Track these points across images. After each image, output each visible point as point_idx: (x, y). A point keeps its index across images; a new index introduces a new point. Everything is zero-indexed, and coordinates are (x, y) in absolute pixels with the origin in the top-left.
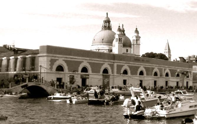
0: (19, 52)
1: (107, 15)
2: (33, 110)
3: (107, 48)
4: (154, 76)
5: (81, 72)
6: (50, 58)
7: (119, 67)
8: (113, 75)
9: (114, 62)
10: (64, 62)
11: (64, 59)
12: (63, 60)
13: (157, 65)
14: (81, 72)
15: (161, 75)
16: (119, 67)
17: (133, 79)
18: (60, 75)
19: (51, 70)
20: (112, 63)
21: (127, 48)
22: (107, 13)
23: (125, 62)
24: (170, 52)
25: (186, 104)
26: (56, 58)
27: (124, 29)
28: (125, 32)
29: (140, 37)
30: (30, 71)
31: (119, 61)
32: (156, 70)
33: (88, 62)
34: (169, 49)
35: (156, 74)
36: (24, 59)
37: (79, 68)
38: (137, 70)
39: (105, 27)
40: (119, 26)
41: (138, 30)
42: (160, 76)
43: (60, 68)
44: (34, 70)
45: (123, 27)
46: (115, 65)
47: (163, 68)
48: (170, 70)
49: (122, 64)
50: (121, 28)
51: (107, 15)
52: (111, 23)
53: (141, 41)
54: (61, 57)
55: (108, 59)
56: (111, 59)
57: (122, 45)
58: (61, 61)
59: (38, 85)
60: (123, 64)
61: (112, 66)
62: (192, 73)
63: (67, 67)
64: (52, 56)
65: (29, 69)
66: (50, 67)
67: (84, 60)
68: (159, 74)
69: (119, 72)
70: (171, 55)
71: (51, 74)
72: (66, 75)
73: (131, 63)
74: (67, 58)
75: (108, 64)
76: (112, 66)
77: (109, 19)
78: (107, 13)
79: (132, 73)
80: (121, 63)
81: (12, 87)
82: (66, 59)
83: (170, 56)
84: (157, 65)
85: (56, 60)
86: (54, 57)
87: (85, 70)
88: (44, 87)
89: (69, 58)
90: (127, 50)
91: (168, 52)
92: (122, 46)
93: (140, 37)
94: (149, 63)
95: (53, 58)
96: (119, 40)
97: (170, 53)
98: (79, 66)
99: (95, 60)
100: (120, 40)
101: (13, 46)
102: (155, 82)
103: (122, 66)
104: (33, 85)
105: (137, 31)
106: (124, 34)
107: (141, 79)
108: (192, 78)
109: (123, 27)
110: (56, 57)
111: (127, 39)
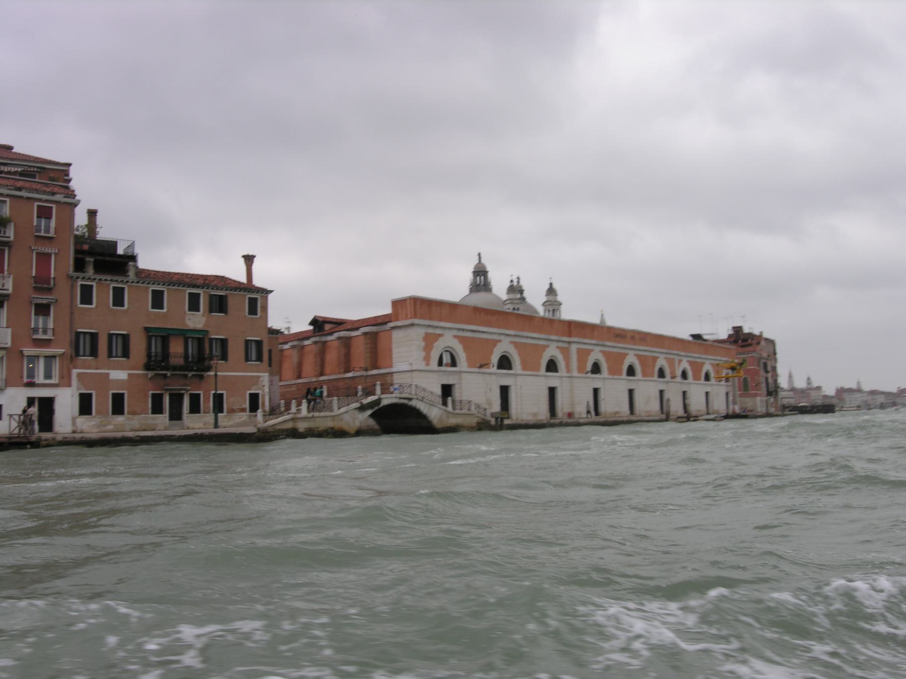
0: (327, 327)
7: (583, 355)
8: (568, 375)
9: (570, 342)
11: (455, 333)
12: (455, 337)
13: (664, 351)
16: (583, 355)
17: (473, 421)
19: (428, 364)
20: (566, 345)
22: (479, 254)
26: (438, 331)
28: (525, 294)
30: (366, 370)
31: (581, 340)
32: (661, 362)
35: (661, 374)
36: (347, 343)
37: (492, 358)
40: (512, 281)
41: (555, 286)
44: (378, 368)
45: (518, 282)
46: (574, 348)
48: (690, 363)
50: (515, 284)
52: (490, 275)
54: (450, 328)
55: (557, 335)
56: (564, 335)
59: (406, 401)
64: (429, 326)
65: (363, 365)
66: (423, 354)
67: (502, 338)
69: (581, 369)
73: (608, 343)
74: (463, 330)
75: (558, 347)
76: (565, 352)
77: (484, 267)
78: (479, 254)
80: (588, 343)
81: (339, 408)
82: (461, 334)
84: (664, 351)
86: (432, 326)
87: (505, 363)
88: (423, 407)
89: (468, 330)
94: (647, 346)
95: (430, 331)
99: (527, 337)
101: (288, 328)
103: (589, 352)
104: (394, 401)
109: (518, 282)
110: (437, 327)
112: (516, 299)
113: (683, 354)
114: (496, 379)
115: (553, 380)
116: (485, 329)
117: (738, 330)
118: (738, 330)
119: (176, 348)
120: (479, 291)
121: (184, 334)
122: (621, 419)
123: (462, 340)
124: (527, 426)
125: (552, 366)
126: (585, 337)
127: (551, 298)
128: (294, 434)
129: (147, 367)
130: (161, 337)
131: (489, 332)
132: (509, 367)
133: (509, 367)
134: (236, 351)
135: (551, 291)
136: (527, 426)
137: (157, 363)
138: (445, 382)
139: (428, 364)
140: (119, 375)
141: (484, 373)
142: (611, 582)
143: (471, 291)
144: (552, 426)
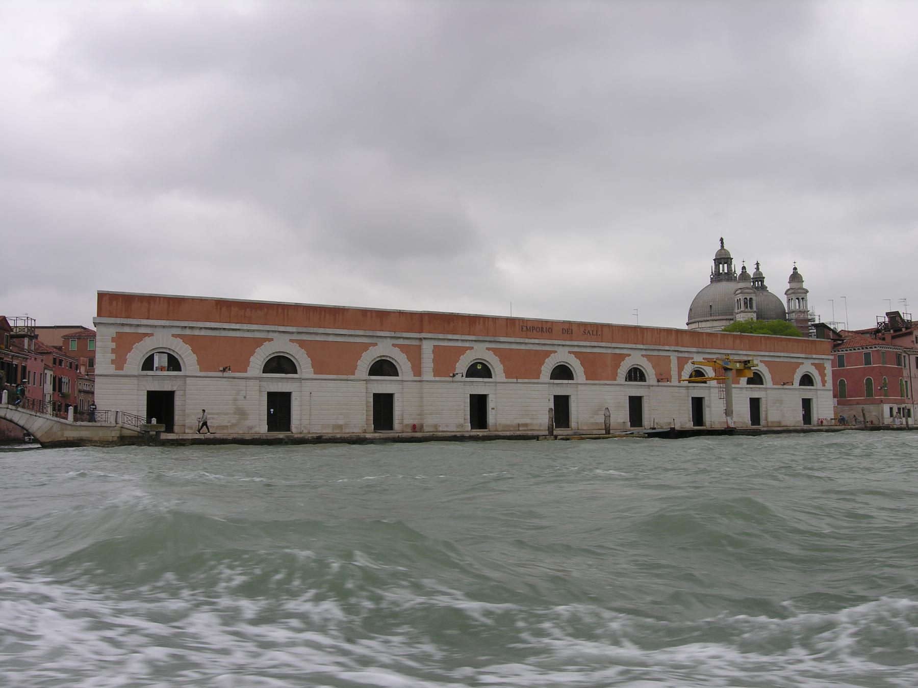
2: (514, 465)
4: (552, 381)
5: (143, 370)
10: (573, 356)
14: (143, 370)
17: (114, 434)
19: (120, 367)
20: (416, 343)
22: (722, 240)
23: (473, 338)
25: (481, 494)
29: (807, 292)
31: (441, 336)
33: (812, 364)
42: (658, 381)
46: (427, 348)
49: (459, 344)
60: (800, 361)
61: (414, 355)
63: (432, 365)
71: (116, 380)
72: (712, 390)
76: (414, 355)
77: (727, 253)
78: (722, 240)
79: (509, 373)
93: (807, 292)
96: (745, 303)
98: (542, 363)
102: (807, 404)
106: (764, 288)
108: (829, 384)
110: (138, 326)
112: (747, 288)
113: (694, 350)
114: (742, 395)
116: (226, 326)
117: (894, 316)
118: (894, 316)
120: (720, 281)
122: (530, 433)
124: (319, 440)
125: (383, 368)
126: (454, 332)
127: (795, 285)
135: (795, 277)
136: (319, 440)
138: (156, 387)
139: (120, 367)
141: (234, 378)
143: (712, 281)
144: (804, 431)
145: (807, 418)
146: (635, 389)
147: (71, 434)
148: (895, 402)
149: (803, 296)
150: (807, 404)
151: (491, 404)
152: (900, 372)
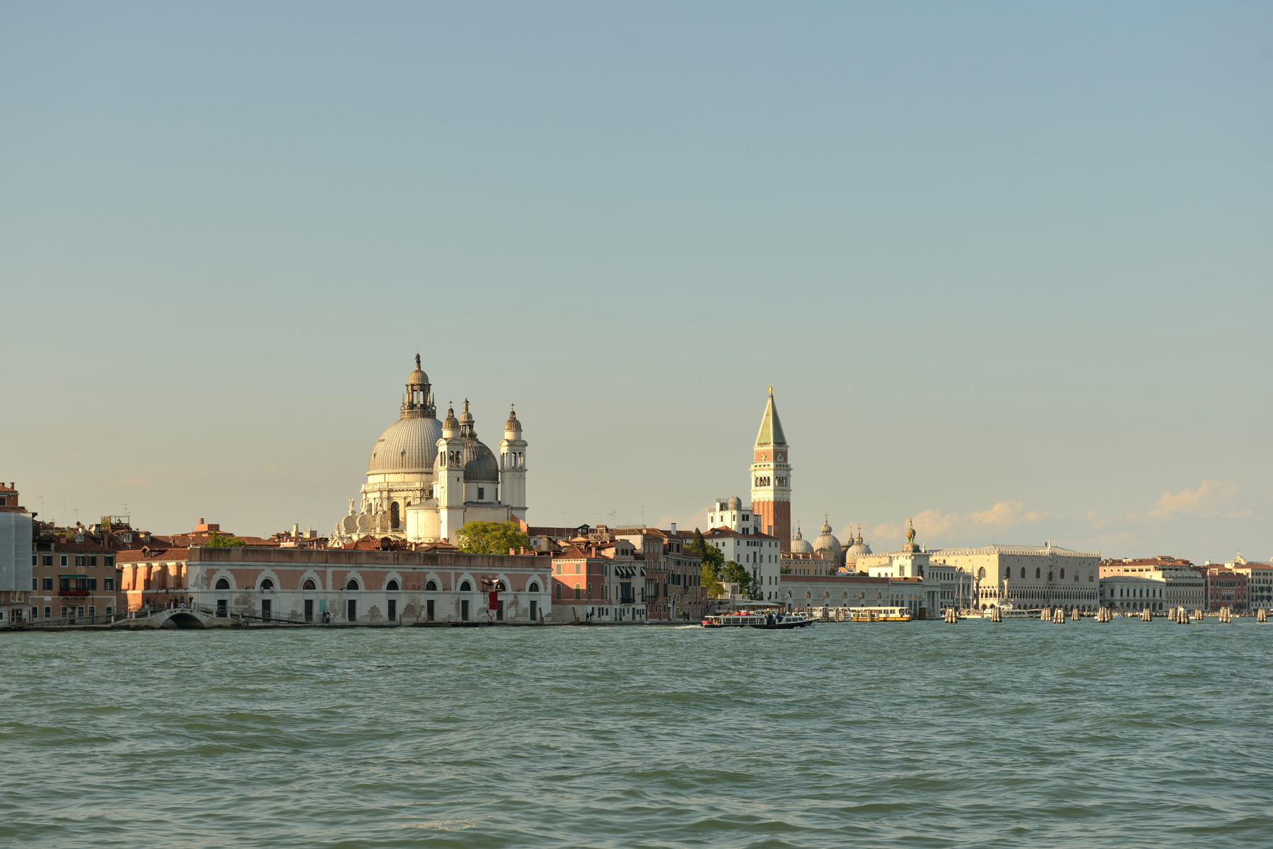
1: (419, 362)
3: (418, 485)
6: (205, 568)
15: (446, 588)
16: (338, 576)
18: (223, 595)
21: (481, 485)
22: (418, 357)
24: (785, 455)
27: (469, 416)
34: (779, 440)
35: (466, 586)
38: (383, 580)
39: (412, 406)
43: (223, 584)
46: (330, 571)
47: (453, 573)
51: (419, 362)
53: (531, 459)
57: (461, 474)
58: (223, 571)
61: (323, 575)
62: (549, 581)
68: (439, 585)
70: (788, 468)
76: (323, 575)
78: (418, 357)
80: (342, 567)
83: (783, 474)
85: (214, 572)
87: (267, 584)
90: (481, 492)
91: (776, 453)
92: (462, 479)
96: (451, 458)
97: (786, 459)
100: (454, 458)
105: (515, 425)
106: (473, 436)
107: (464, 598)
111: (483, 453)
114: (423, 598)
115: (310, 595)
119: (73, 585)
121: (74, 577)
123: (232, 571)
125: (310, 585)
128: (128, 628)
129: (60, 594)
130: (65, 582)
131: (252, 565)
132: (537, 590)
133: (537, 590)
134: (100, 585)
137: (64, 591)
140: (48, 598)
142: (567, 711)
143: (38, 527)
145: (533, 616)
146: (430, 596)
147: (216, 623)
148: (596, 603)
149: (520, 449)
150: (533, 604)
151: (358, 606)
152: (602, 579)
